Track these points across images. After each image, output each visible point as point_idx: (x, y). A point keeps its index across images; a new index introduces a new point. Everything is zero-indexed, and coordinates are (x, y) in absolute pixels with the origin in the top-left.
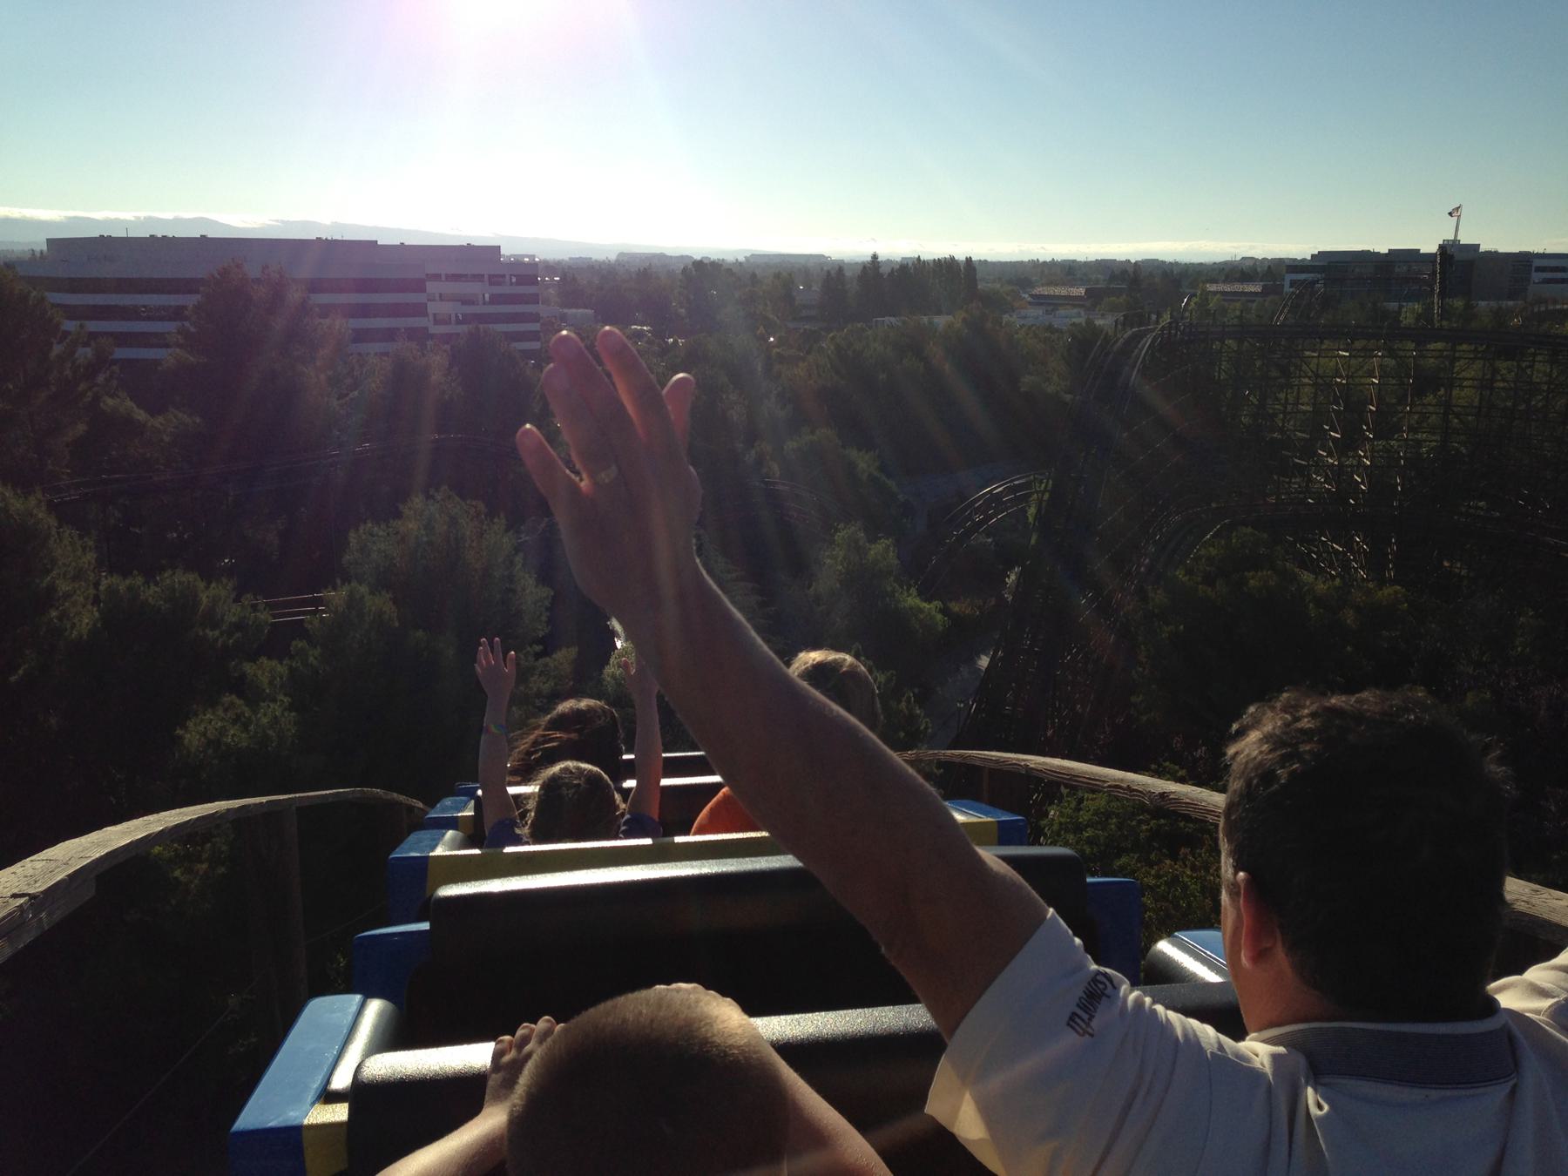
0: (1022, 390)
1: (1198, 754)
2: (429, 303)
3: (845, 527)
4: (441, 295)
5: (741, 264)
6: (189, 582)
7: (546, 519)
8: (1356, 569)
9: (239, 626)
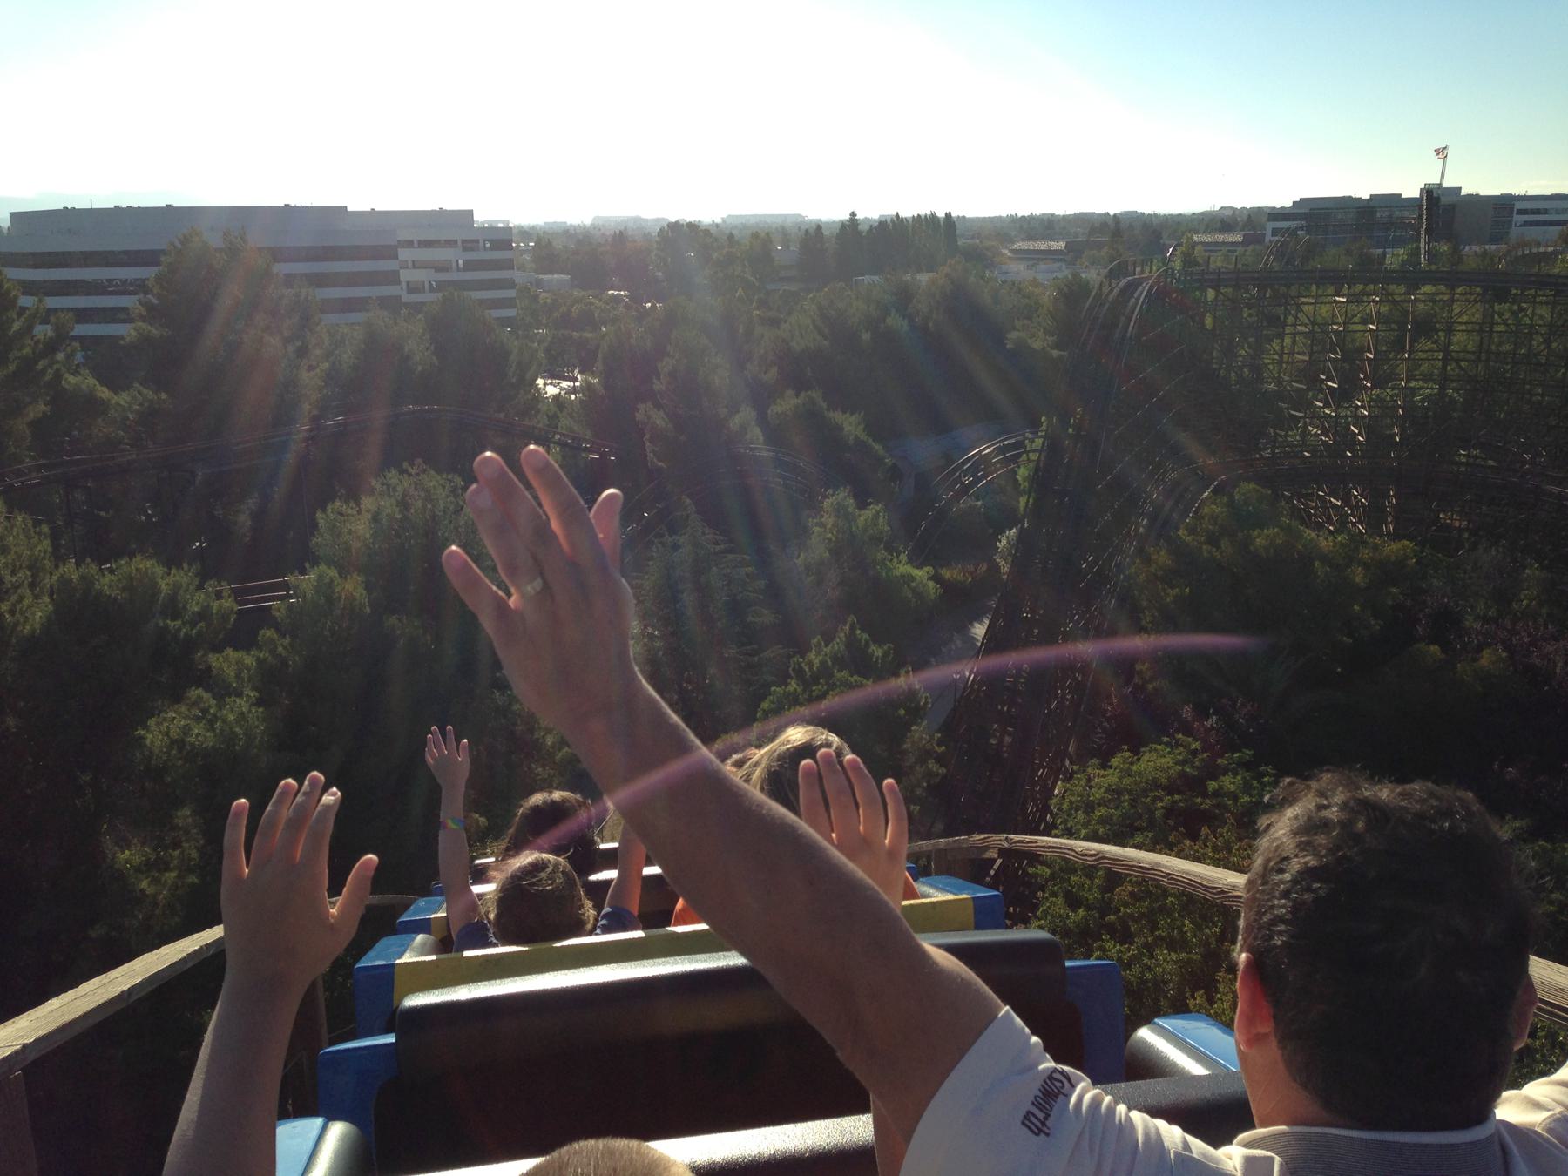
0: (1008, 346)
3: (834, 492)
4: (413, 262)
5: (717, 225)
6: (146, 569)
8: (1353, 524)
9: (203, 615)
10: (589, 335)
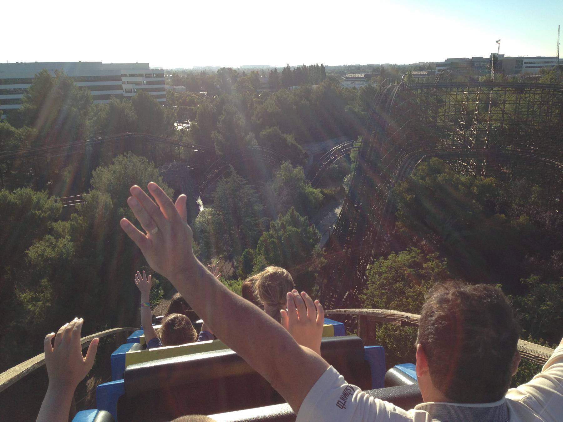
0: (346, 111)
1: (423, 243)
2: (123, 85)
4: (127, 82)
5: (239, 69)
7: (171, 164)
9: (51, 209)
10: (193, 108)
